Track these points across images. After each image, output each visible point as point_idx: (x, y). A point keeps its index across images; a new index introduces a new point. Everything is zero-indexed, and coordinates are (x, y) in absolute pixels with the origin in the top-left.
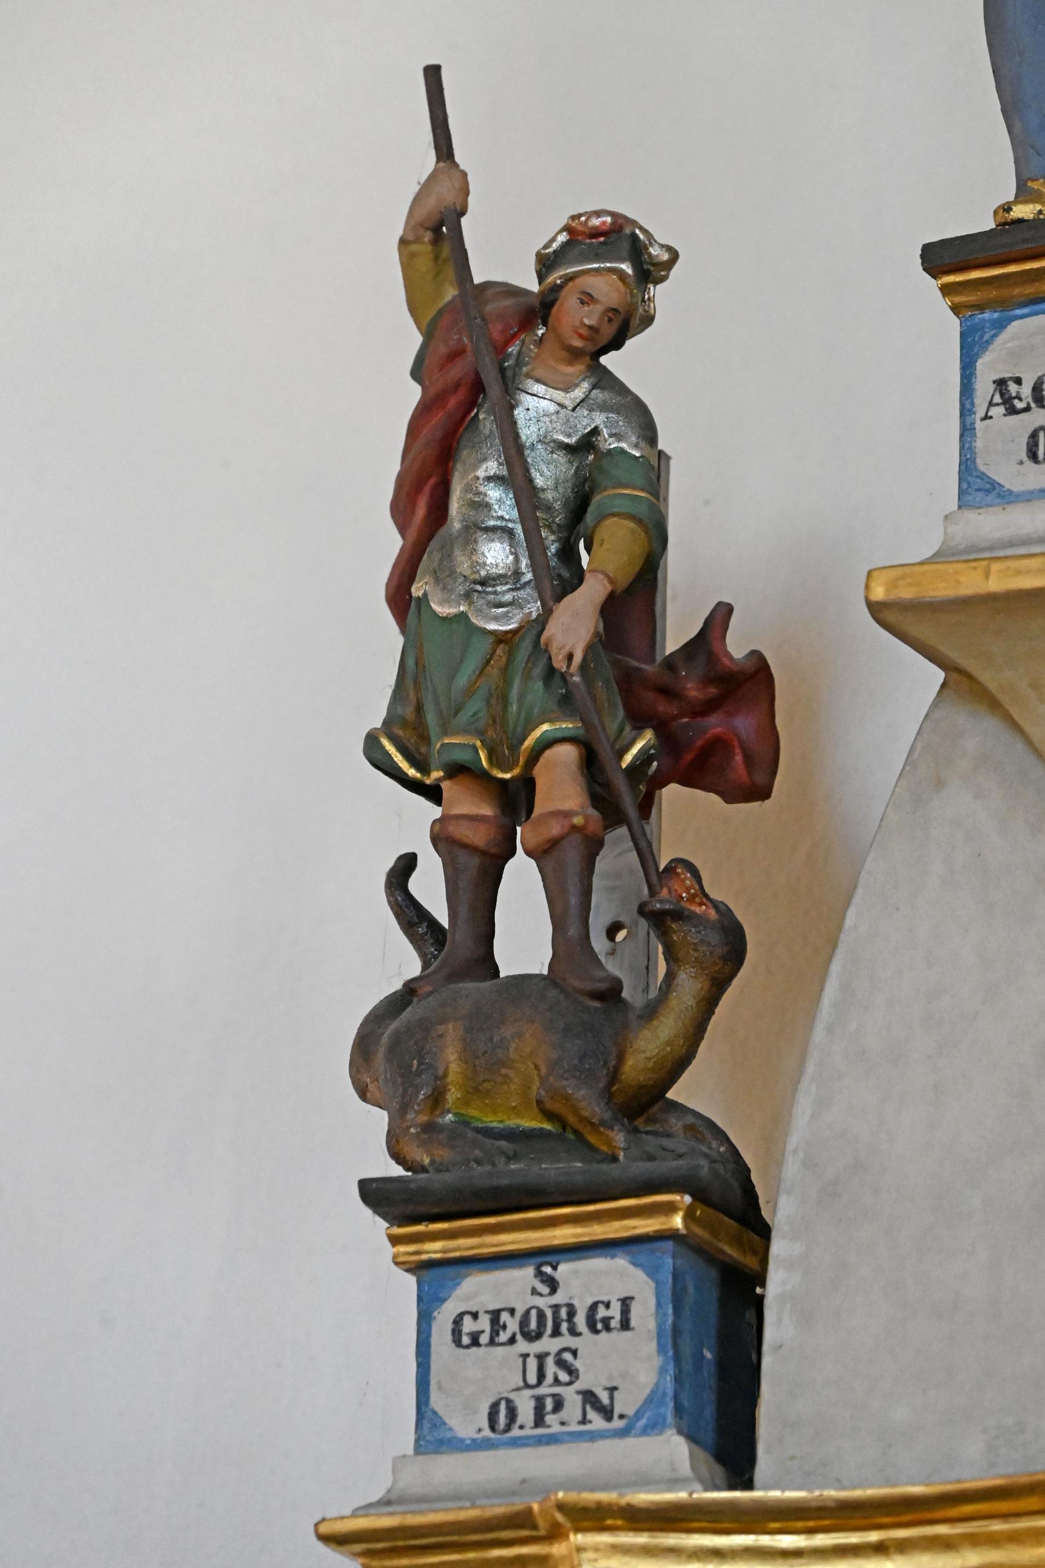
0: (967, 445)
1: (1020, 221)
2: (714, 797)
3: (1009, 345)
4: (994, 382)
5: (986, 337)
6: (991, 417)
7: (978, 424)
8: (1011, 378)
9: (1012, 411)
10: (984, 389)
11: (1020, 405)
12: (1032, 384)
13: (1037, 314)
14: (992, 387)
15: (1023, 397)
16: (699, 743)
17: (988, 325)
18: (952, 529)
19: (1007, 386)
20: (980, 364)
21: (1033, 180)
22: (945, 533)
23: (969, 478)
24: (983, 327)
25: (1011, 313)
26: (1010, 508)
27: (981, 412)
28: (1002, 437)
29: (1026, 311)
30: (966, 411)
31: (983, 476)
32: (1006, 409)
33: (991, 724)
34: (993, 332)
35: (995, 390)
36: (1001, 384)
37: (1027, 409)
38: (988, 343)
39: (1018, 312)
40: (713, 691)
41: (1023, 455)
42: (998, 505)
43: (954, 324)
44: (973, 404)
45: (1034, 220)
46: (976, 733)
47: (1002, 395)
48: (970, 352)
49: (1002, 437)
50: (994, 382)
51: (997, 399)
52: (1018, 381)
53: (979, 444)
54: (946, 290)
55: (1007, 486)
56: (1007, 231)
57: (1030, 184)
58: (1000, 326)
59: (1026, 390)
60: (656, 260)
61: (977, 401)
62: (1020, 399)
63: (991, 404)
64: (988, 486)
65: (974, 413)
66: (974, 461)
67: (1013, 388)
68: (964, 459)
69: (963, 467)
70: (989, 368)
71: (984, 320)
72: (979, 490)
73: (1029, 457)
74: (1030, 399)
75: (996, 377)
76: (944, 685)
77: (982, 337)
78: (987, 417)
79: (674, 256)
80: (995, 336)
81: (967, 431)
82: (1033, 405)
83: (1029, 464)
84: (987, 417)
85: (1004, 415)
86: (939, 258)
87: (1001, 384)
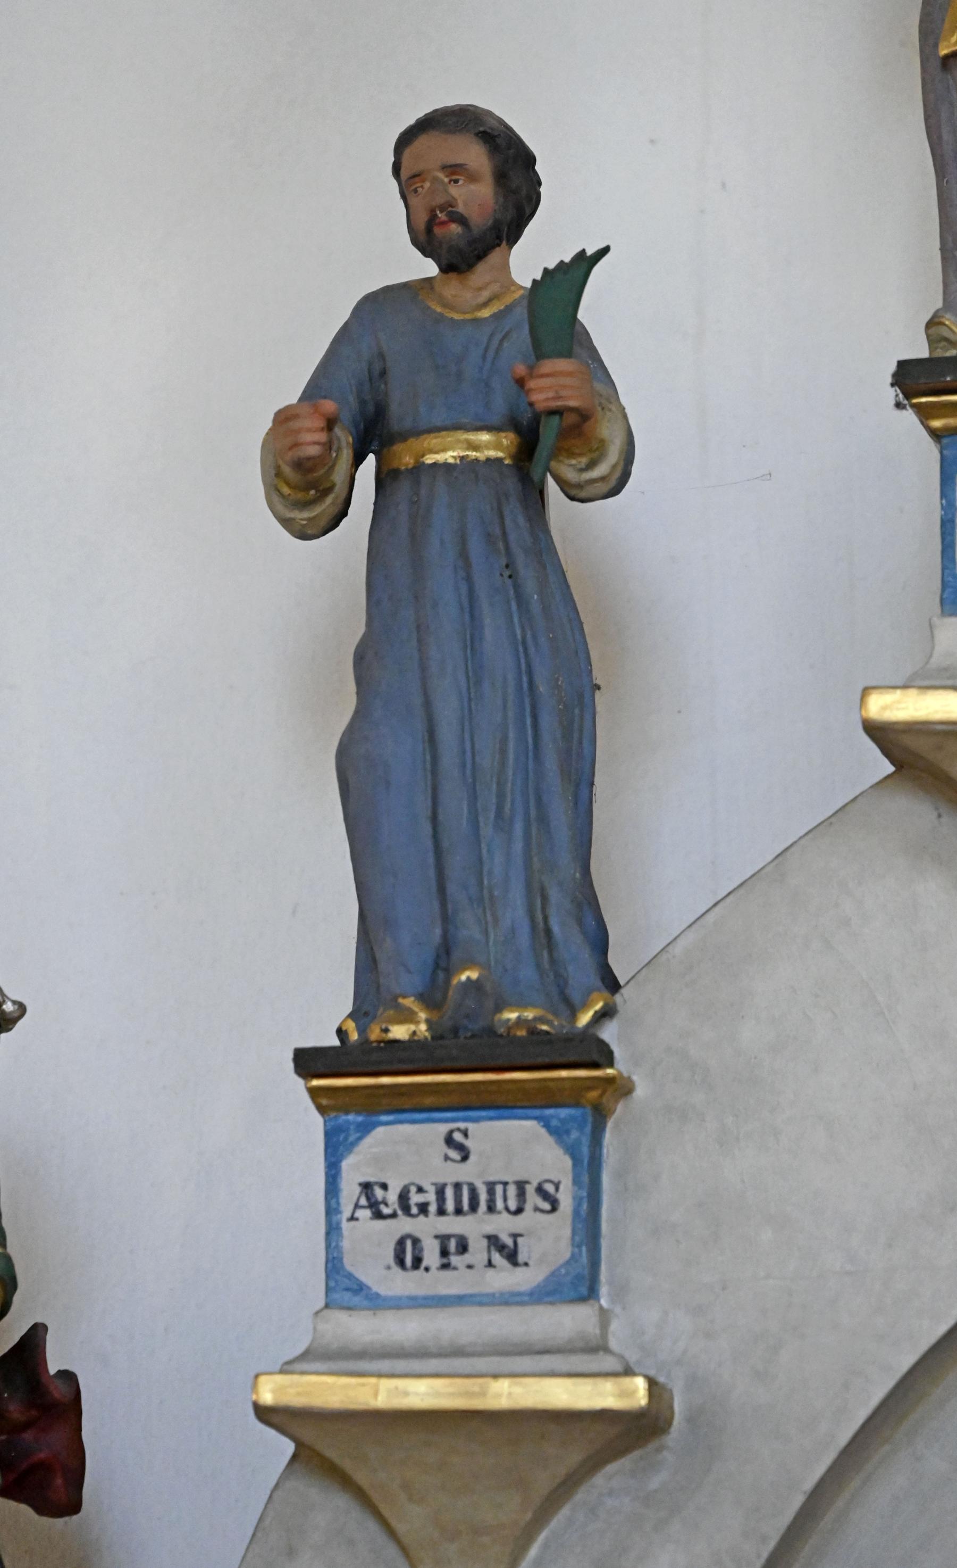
0: (333, 1244)
1: (396, 1041)
2: (25, 1509)
3: (375, 1150)
4: (360, 1184)
5: (351, 1139)
6: (357, 1219)
7: (345, 1225)
8: (376, 1183)
9: (378, 1215)
10: (349, 1190)
11: (386, 1211)
12: (398, 1190)
13: (401, 1122)
14: (358, 1189)
15: (390, 1202)
16: (24, 1466)
17: (352, 1127)
18: (322, 1327)
19: (372, 1190)
20: (345, 1164)
21: (404, 997)
22: (315, 1329)
23: (338, 1278)
24: (348, 1129)
25: (374, 1119)
26: (380, 1314)
27: (347, 1213)
28: (367, 1243)
29: (390, 1118)
30: (331, 1210)
31: (350, 1276)
32: (373, 1213)
33: (341, 1501)
34: (358, 1135)
35: (361, 1193)
36: (367, 1187)
37: (394, 1215)
38: (354, 1144)
39: (384, 1118)
40: (34, 1413)
41: (390, 1260)
42: (369, 1309)
43: (317, 1122)
44: (338, 1204)
45: (409, 1041)
46: (329, 1508)
47: (368, 1199)
48: (336, 1148)
49: (369, 1244)
50: (360, 1184)
51: (363, 1201)
52: (384, 1187)
53: (346, 1244)
54: (314, 1093)
55: (376, 1288)
56: (381, 1048)
57: (400, 1000)
58: (365, 1129)
59: (392, 1196)
60: (8, 1017)
61: (343, 1201)
62: (386, 1205)
63: (357, 1206)
64: (355, 1287)
65: (340, 1212)
66: (341, 1260)
67: (379, 1193)
68: (331, 1257)
69: (330, 1265)
70: (354, 1170)
71: (348, 1122)
72: (347, 1289)
73: (396, 1263)
74: (396, 1206)
75: (363, 1179)
76: (295, 1457)
77: (346, 1139)
78: (352, 1218)
79: (22, 1009)
80: (360, 1139)
81: (332, 1230)
82: (400, 1212)
83: (396, 1269)
84: (352, 1218)
85: (371, 1219)
86: (308, 1062)
87: (367, 1187)
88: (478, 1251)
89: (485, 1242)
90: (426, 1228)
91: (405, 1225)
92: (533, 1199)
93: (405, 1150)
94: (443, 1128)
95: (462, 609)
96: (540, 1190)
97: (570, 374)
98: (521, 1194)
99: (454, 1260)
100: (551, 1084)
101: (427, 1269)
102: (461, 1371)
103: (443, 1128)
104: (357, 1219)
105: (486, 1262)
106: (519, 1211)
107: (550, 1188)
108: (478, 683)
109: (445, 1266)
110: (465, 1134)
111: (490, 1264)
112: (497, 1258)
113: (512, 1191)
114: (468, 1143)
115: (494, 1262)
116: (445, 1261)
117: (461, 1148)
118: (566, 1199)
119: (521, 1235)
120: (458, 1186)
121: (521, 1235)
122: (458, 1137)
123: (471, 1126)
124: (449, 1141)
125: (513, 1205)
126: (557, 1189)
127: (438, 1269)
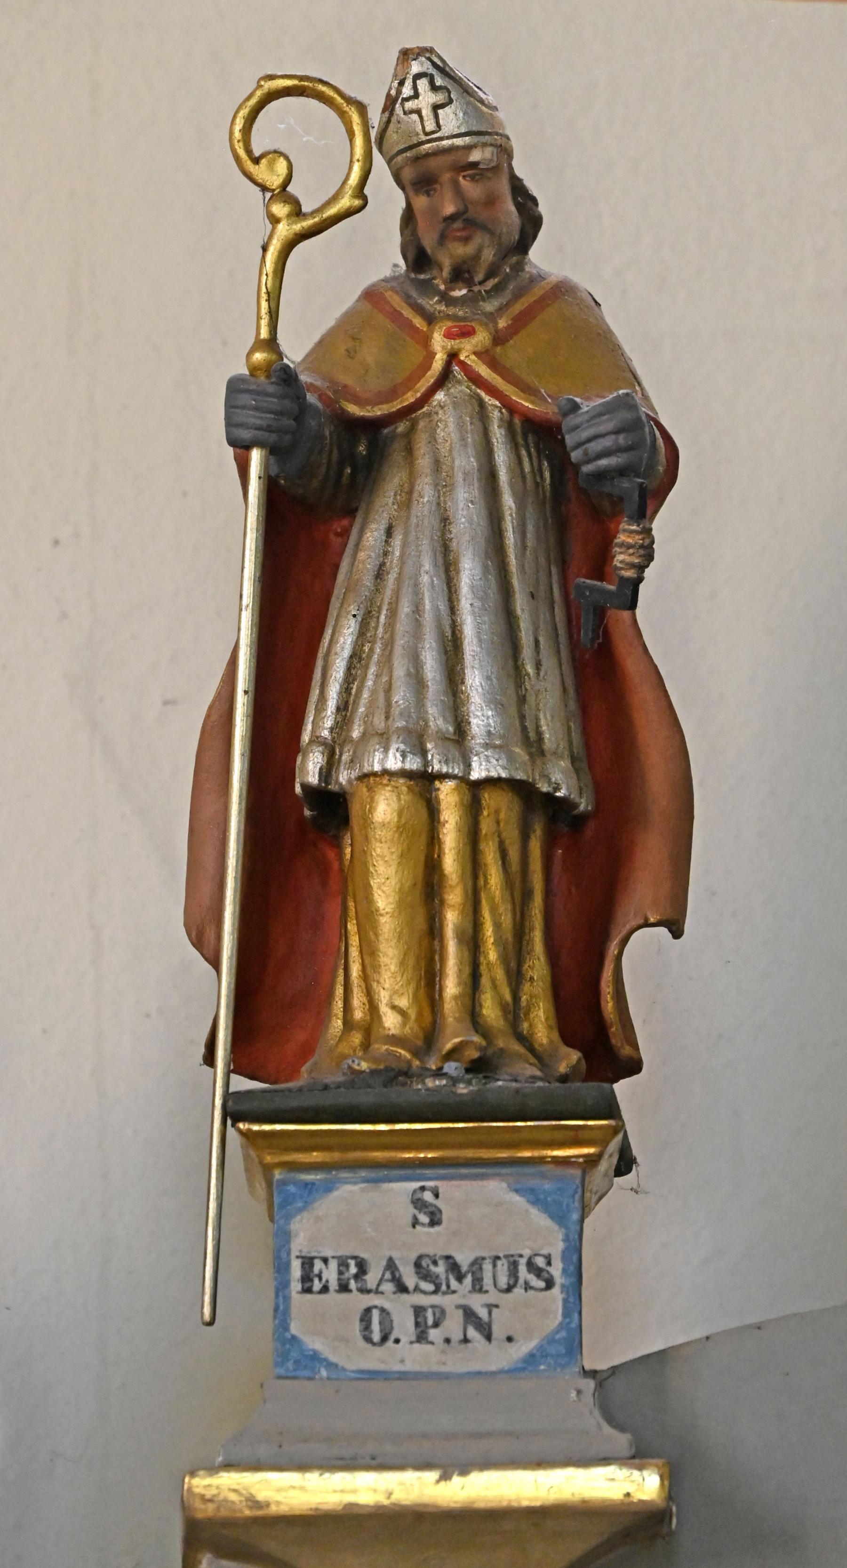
70: (303, 1235)
88: (454, 1325)
92: (523, 1273)
96: (531, 1266)
98: (514, 1267)
105: (461, 1337)
106: (509, 1289)
107: (540, 1262)
111: (466, 1340)
112: (472, 1333)
113: (503, 1267)
116: (307, 1285)
118: (556, 1271)
119: (497, 1306)
121: (497, 1306)
122: (428, 1196)
123: (442, 1186)
124: (418, 1203)
125: (503, 1281)
126: (437, 1196)
127: (298, 1292)
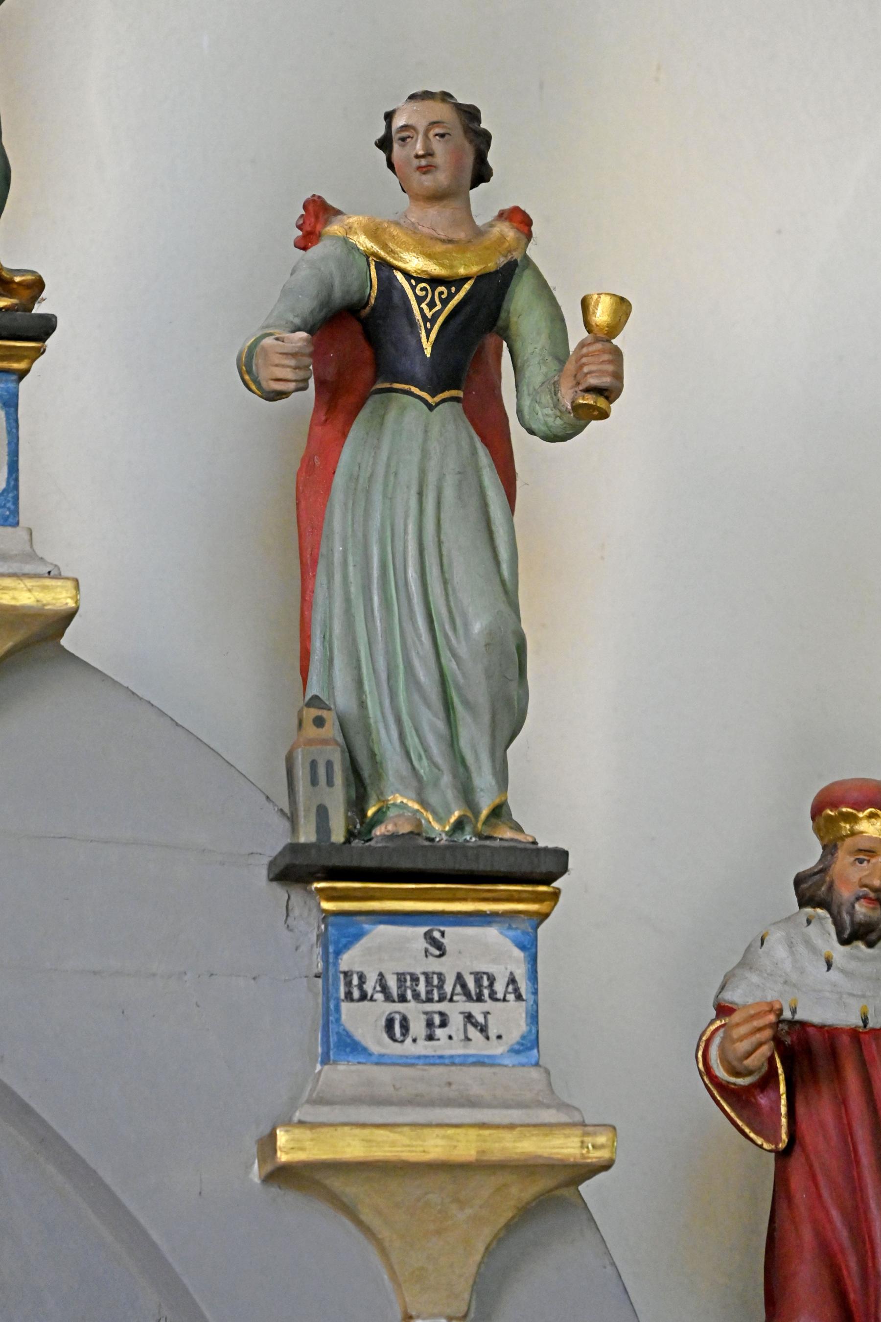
6: (375, 1001)
51: (378, 988)
88: (456, 1021)
89: (461, 1017)
90: (413, 1010)
91: (429, 1007)
93: (388, 948)
94: (425, 929)
95: (396, 474)
97: (749, 1054)
99: (439, 1032)
100: (514, 893)
101: (414, 1040)
102: (447, 1121)
103: (425, 929)
104: (375, 1001)
108: (856, 1208)
109: (430, 1038)
110: (443, 934)
114: (444, 941)
115: (470, 1036)
117: (439, 946)
119: (488, 1013)
120: (426, 974)
122: (436, 934)
124: (428, 936)
126: (426, 951)
